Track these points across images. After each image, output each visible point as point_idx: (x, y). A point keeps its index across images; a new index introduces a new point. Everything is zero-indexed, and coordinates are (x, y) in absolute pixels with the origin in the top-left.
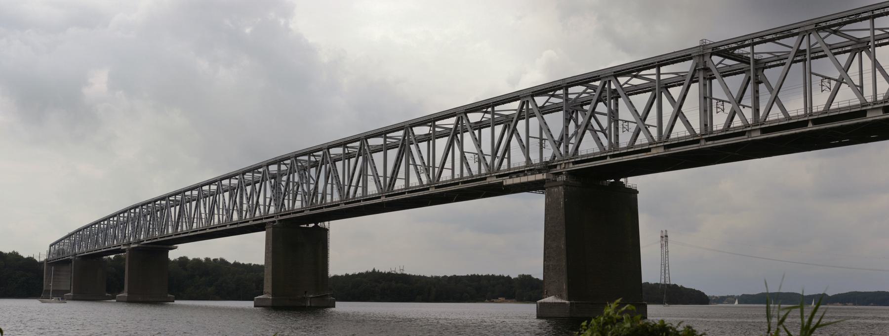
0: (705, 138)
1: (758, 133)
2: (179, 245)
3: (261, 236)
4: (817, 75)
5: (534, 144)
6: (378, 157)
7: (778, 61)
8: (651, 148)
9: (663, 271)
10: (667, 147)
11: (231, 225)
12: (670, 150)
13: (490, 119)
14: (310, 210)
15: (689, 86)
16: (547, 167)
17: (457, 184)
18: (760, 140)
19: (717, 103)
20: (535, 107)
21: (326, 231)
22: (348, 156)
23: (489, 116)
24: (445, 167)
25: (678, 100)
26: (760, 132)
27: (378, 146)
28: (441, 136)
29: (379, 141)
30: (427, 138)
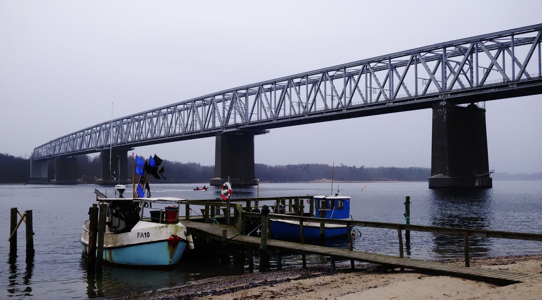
2: (271, 130)
3: (213, 139)
5: (329, 99)
6: (220, 105)
7: (402, 64)
10: (394, 102)
11: (116, 145)
14: (116, 145)
15: (361, 75)
17: (414, 99)
21: (483, 111)
22: (205, 105)
25: (523, 65)
27: (219, 99)
29: (221, 97)
30: (245, 95)
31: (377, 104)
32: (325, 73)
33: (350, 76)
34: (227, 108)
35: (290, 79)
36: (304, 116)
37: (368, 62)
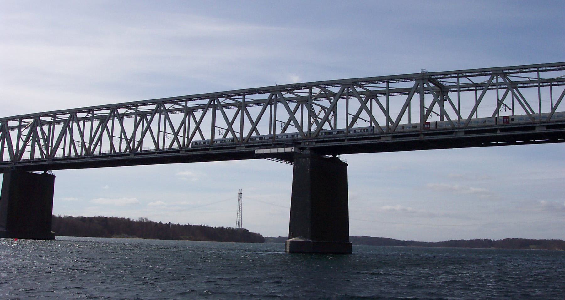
0: (423, 134)
1: (463, 134)
4: (351, 115)
6: (14, 134)
7: (199, 108)
8: (236, 147)
9: (239, 210)
12: (396, 139)
13: (91, 117)
14: (317, 142)
16: (294, 141)
18: (463, 138)
19: (282, 124)
20: (164, 109)
21: (345, 165)
23: (91, 115)
24: (59, 147)
26: (545, 128)
28: (59, 122)
31: (170, 150)
32: (161, 104)
33: (144, 115)
34: (24, 138)
35: (73, 112)
36: (381, 139)
37: (39, 116)
